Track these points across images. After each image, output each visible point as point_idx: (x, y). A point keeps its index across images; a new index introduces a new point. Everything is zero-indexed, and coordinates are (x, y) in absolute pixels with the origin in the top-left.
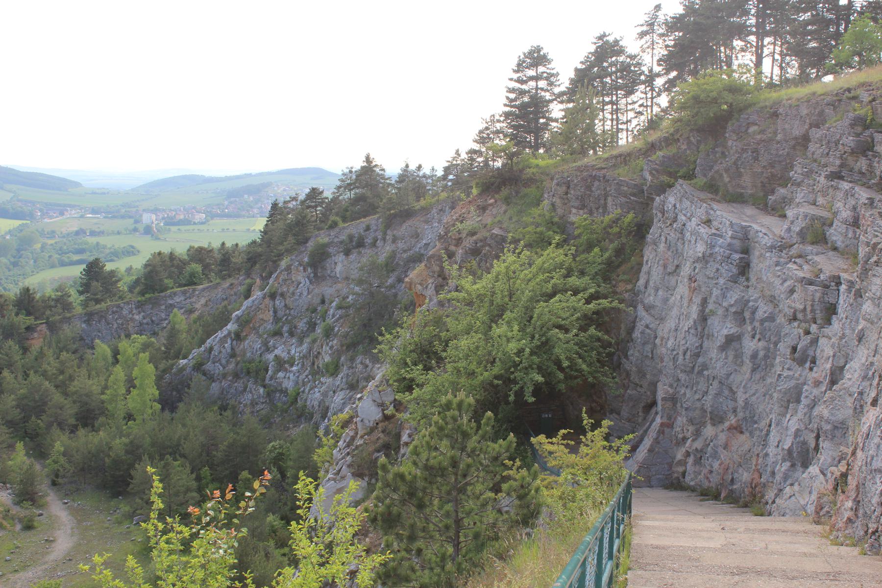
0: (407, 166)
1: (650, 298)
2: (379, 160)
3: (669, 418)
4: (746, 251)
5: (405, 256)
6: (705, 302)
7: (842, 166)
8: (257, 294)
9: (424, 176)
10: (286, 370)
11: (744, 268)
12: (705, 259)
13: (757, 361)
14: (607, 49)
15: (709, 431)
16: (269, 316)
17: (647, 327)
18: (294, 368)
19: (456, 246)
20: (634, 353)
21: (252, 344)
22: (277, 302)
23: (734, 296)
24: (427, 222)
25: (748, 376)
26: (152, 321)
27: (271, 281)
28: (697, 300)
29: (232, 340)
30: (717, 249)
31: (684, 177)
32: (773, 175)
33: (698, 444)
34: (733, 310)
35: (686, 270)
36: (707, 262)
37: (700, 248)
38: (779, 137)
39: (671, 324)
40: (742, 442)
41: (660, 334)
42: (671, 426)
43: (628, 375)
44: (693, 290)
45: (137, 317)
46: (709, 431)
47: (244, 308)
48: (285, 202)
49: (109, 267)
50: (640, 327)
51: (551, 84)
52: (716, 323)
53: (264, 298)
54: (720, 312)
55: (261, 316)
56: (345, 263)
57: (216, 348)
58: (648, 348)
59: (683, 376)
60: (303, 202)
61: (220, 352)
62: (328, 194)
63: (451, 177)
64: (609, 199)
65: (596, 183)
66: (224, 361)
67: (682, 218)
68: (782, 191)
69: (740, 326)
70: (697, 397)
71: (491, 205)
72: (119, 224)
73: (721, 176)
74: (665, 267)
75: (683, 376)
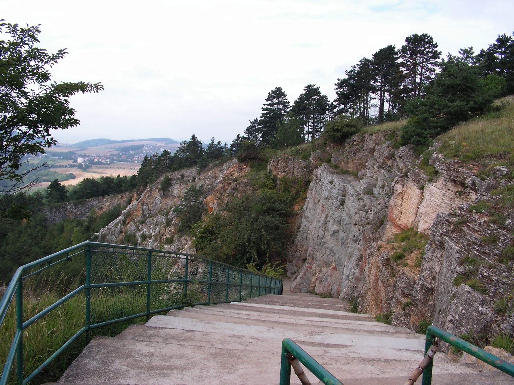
0: (213, 142)
1: (307, 214)
2: (199, 138)
3: (311, 264)
4: (344, 196)
5: (209, 187)
6: (326, 217)
7: (383, 163)
8: (134, 202)
9: (222, 147)
10: (147, 241)
11: (343, 203)
12: (327, 198)
13: (343, 241)
14: (312, 92)
15: (325, 270)
16: (140, 214)
17: (305, 226)
18: (151, 240)
19: (228, 186)
20: (299, 237)
21: (131, 227)
22: (144, 207)
23: (337, 214)
24: (221, 171)
25: (340, 247)
26: (82, 213)
27: (142, 196)
28: (324, 215)
29: (121, 225)
30: (333, 194)
31: (326, 162)
32: (361, 164)
33: (321, 275)
34: (336, 220)
35: (321, 203)
36: (329, 199)
37: (327, 193)
38: (365, 148)
39: (314, 225)
40: (337, 274)
41: (310, 229)
42: (311, 268)
43: (297, 246)
44: (322, 211)
45: (74, 211)
46: (325, 270)
47: (127, 209)
48: (151, 157)
49: (62, 183)
50: (302, 226)
51: (284, 106)
52: (330, 225)
53: (138, 204)
54: (332, 221)
55: (136, 213)
56: (179, 189)
57: (113, 228)
58: (305, 235)
59: (316, 247)
60: (160, 157)
61: (115, 230)
62: (172, 155)
63: (234, 149)
64: (295, 169)
65: (290, 162)
66: (117, 235)
67: (322, 180)
68: (363, 171)
69: (339, 227)
70: (321, 255)
71: (245, 168)
72: (65, 163)
73: (341, 163)
74: (314, 200)
75: (316, 247)
